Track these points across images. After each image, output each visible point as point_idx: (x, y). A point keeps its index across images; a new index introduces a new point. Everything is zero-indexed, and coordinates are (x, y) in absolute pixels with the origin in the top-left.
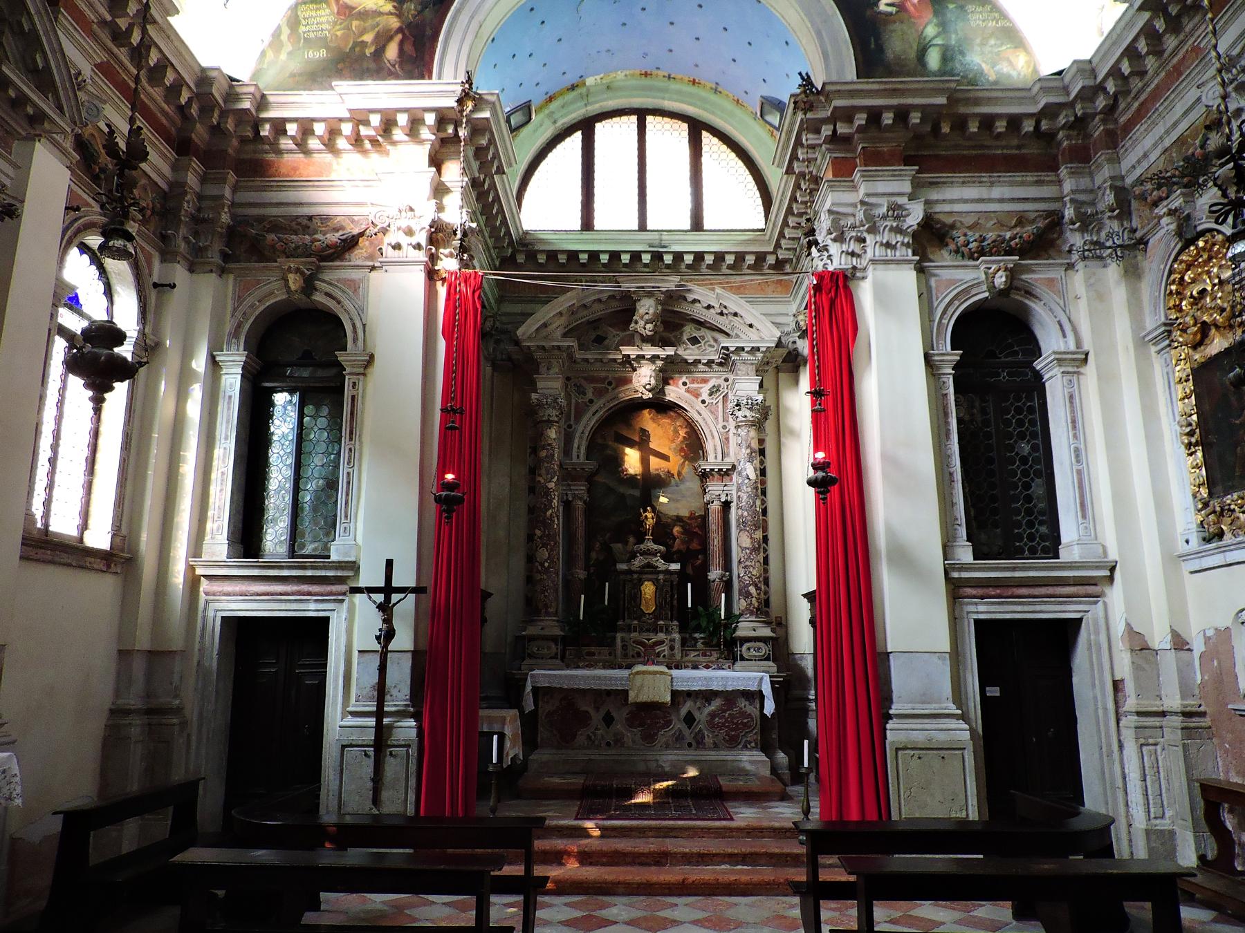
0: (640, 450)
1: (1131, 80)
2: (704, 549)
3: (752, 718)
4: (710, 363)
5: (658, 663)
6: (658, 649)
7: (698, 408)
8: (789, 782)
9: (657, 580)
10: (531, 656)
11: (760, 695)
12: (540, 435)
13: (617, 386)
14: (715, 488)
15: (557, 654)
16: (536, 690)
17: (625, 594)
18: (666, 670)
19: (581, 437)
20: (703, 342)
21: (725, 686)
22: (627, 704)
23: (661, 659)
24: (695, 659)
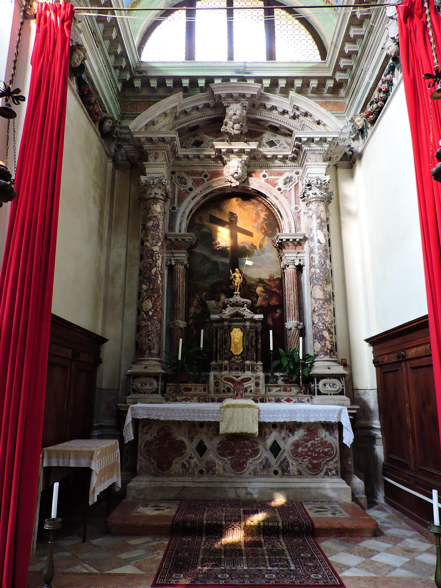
0: (230, 228)
2: (281, 305)
3: (332, 448)
4: (285, 158)
5: (247, 397)
6: (246, 385)
7: (275, 194)
8: (365, 506)
9: (245, 327)
10: (135, 391)
11: (340, 426)
12: (148, 209)
13: (212, 178)
14: (290, 255)
15: (157, 389)
16: (136, 422)
17: (217, 339)
18: (253, 403)
19: (182, 216)
20: (278, 145)
21: (308, 418)
22: (218, 434)
23: (248, 394)
24: (278, 393)
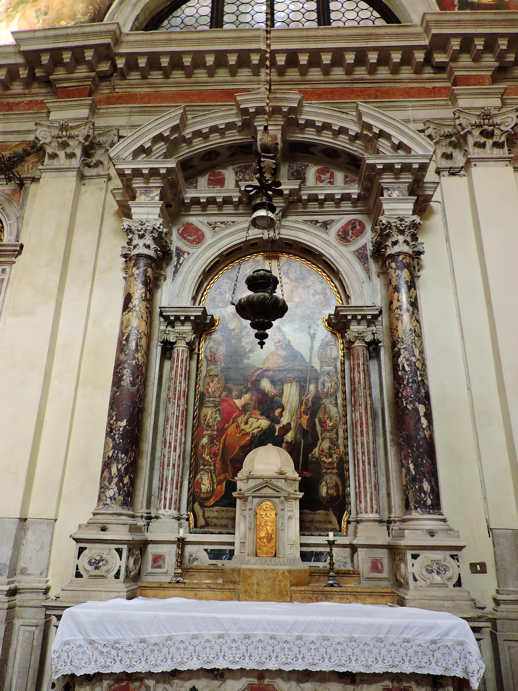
1: (36, 85)
